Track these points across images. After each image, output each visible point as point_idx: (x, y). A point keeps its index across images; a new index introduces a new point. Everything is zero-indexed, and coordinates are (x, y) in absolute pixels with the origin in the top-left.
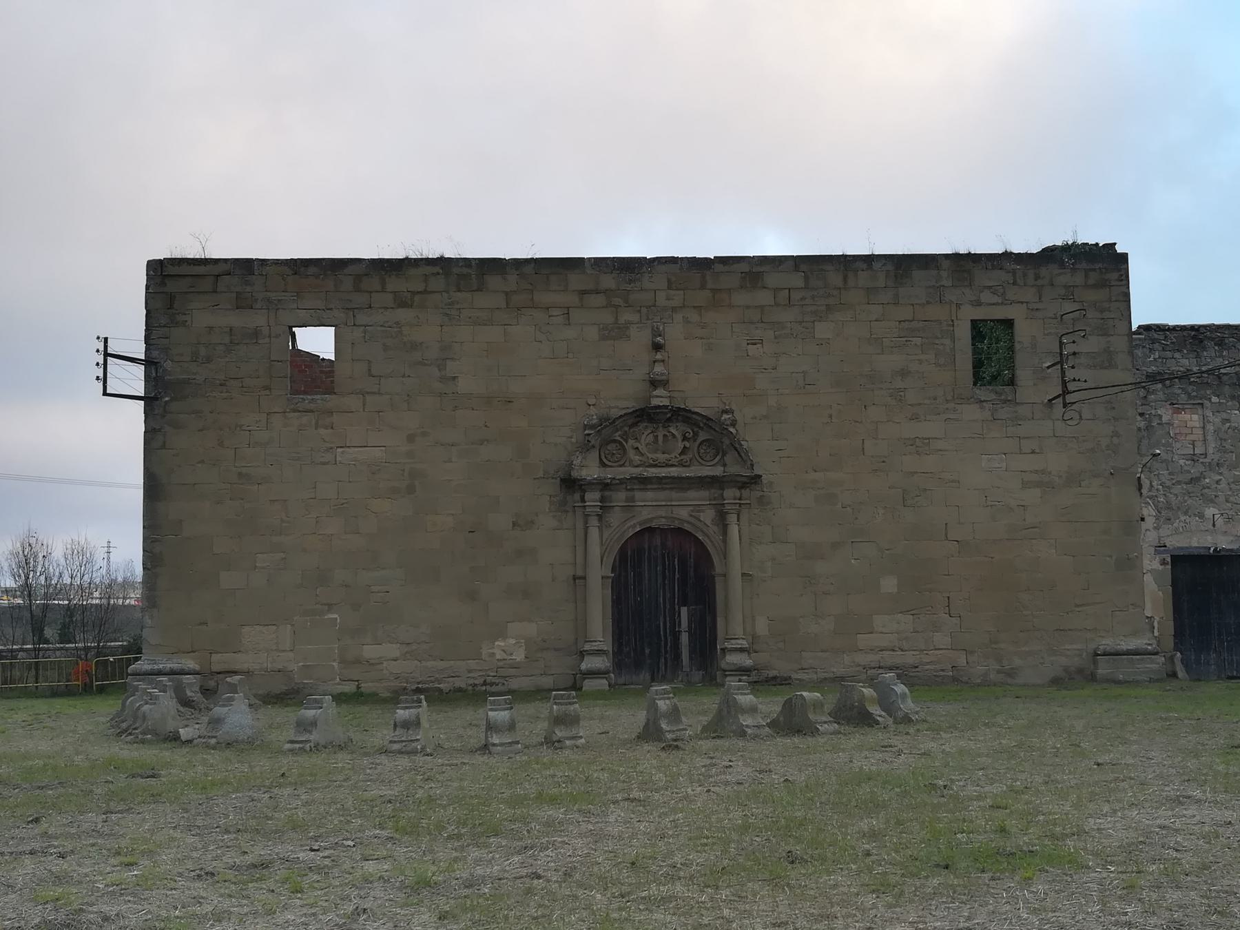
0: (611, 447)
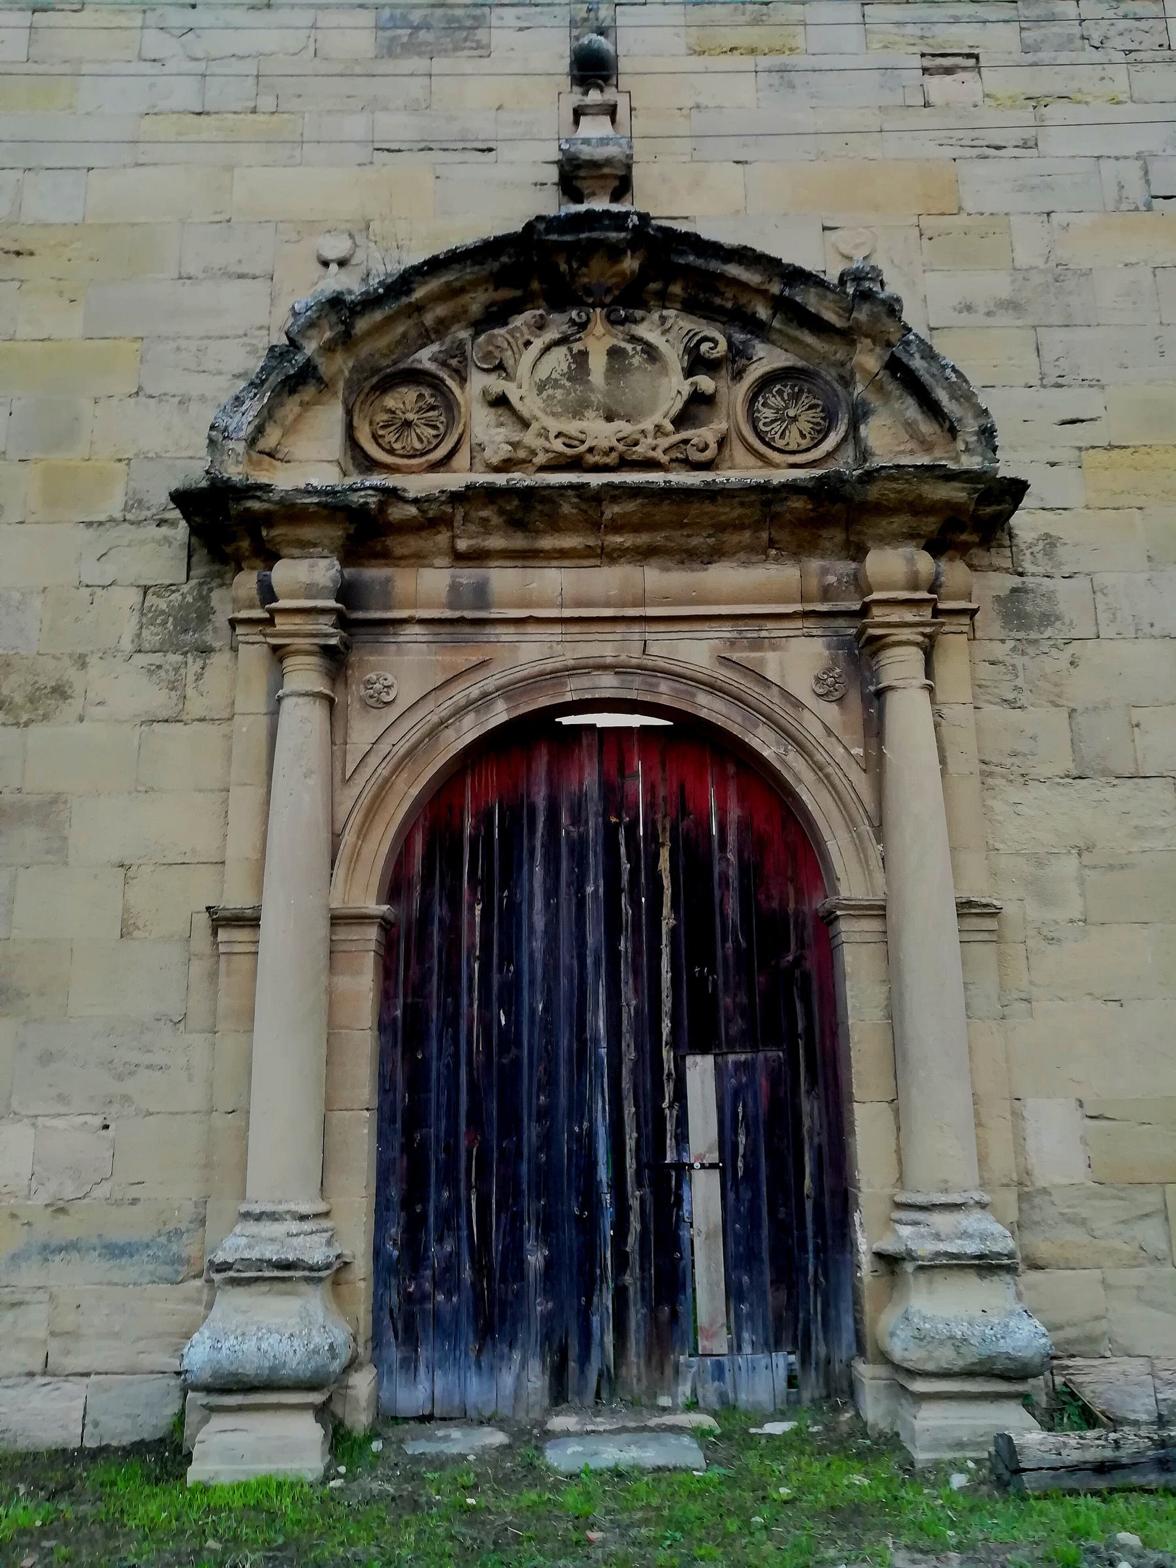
0: (404, 400)
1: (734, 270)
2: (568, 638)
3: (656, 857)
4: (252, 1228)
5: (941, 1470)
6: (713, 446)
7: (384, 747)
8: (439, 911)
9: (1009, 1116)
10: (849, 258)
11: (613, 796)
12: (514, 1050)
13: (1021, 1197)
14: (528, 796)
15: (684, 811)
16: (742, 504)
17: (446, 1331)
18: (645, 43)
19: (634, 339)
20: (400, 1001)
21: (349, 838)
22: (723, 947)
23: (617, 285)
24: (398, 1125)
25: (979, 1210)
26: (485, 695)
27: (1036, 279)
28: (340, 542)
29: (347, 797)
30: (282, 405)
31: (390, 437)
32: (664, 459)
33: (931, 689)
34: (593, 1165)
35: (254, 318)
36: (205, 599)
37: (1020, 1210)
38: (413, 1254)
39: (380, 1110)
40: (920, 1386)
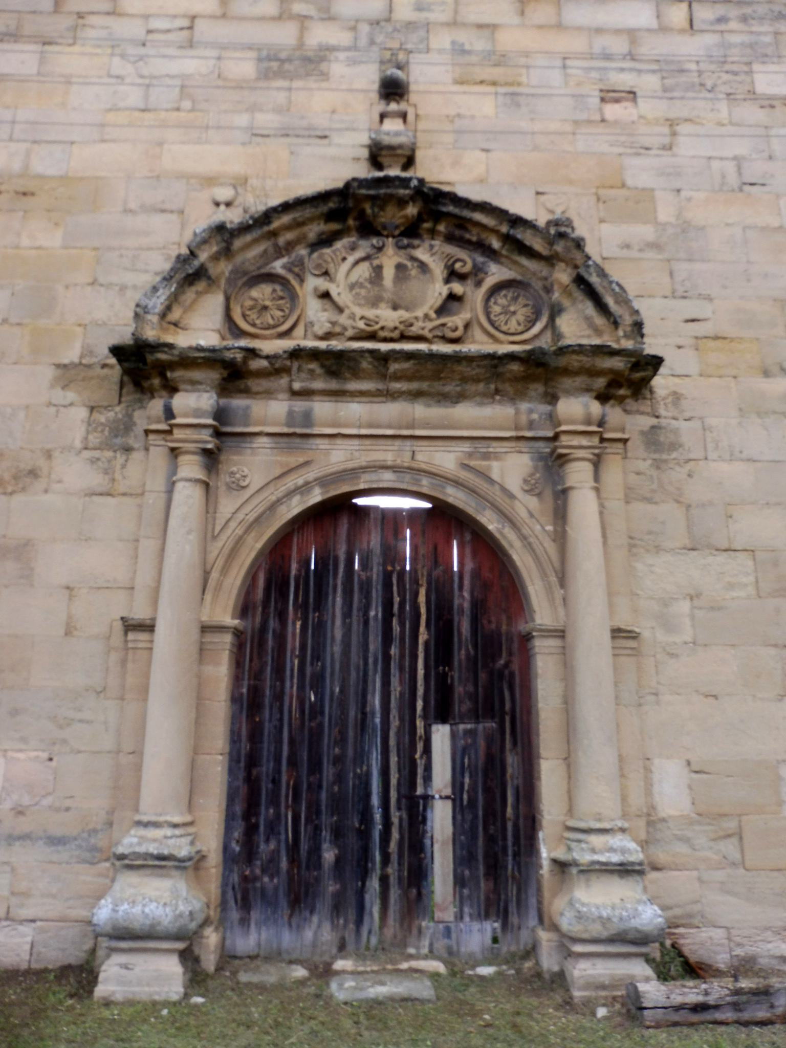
0: (263, 293)
1: (478, 217)
2: (363, 448)
3: (416, 594)
4: (142, 832)
5: (589, 1007)
6: (461, 329)
7: (240, 516)
8: (273, 624)
9: (642, 771)
10: (552, 212)
11: (391, 555)
12: (319, 718)
13: (650, 823)
14: (334, 550)
15: (436, 563)
16: (479, 366)
17: (269, 901)
18: (426, 75)
19: (413, 259)
20: (246, 683)
21: (214, 575)
22: (459, 654)
23: (402, 224)
24: (242, 764)
25: (620, 833)
26: (307, 483)
27: (670, 231)
28: (217, 382)
29: (215, 548)
30: (184, 292)
31: (253, 315)
32: (429, 336)
33: (597, 490)
34: (368, 795)
35: (165, 239)
36: (129, 416)
37: (648, 832)
38: (249, 852)
39: (230, 754)
40: (578, 948)
